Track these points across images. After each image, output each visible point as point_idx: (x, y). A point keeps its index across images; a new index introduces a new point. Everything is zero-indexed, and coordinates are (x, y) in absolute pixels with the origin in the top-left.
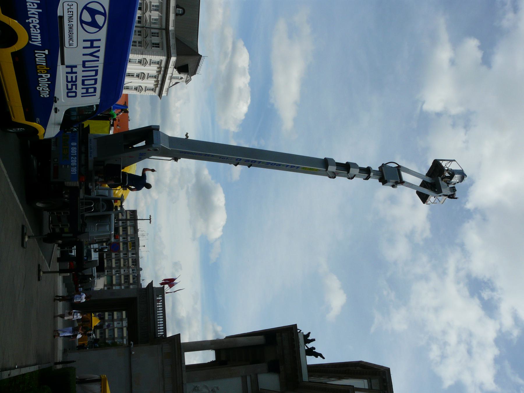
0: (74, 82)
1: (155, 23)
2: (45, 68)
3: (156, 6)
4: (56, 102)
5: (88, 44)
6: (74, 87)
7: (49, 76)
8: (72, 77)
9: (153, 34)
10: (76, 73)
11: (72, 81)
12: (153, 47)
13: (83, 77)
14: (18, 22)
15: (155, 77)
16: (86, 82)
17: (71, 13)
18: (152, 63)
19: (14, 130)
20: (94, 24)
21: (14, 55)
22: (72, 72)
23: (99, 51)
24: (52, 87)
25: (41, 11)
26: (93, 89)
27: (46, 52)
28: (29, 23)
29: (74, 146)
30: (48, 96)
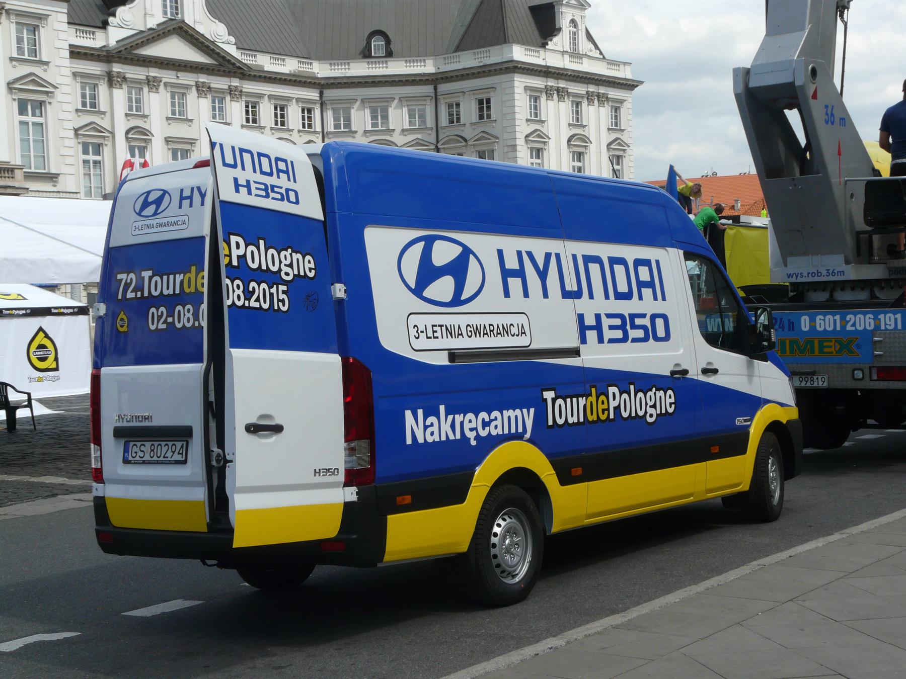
0: (626, 323)
1: (422, 117)
2: (593, 399)
3: (374, 117)
4: (686, 372)
5: (515, 284)
6: (638, 321)
7: (612, 390)
8: (612, 327)
9: (455, 119)
10: (598, 317)
11: (622, 327)
12: (489, 116)
13: (607, 297)
14: (479, 464)
15: (578, 104)
16: (623, 288)
17: (438, 329)
18: (536, 117)
19: (775, 487)
20: (458, 269)
21: (565, 479)
22: (598, 327)
23: (530, 254)
24: (644, 382)
25: (442, 408)
26: (640, 268)
27: (549, 395)
28: (478, 437)
29: (813, 320)
30: (670, 392)
